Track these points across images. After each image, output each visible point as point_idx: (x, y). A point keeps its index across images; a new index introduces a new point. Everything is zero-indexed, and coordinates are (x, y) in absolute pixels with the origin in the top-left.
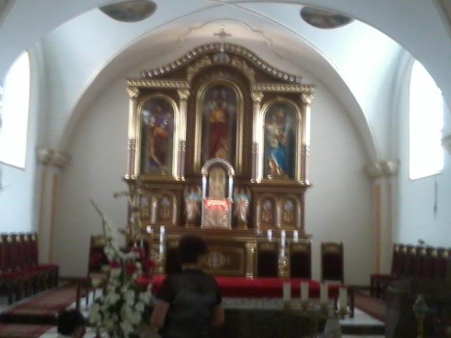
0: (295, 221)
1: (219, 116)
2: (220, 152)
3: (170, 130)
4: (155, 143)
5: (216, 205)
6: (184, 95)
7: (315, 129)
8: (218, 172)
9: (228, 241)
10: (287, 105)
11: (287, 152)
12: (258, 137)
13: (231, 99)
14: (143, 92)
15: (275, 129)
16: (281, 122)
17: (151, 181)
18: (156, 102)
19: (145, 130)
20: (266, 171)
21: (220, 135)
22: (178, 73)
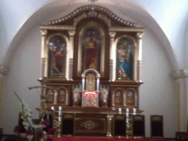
0: (133, 103)
1: (91, 45)
2: (92, 65)
3: (64, 53)
4: (56, 60)
5: (90, 94)
6: (72, 34)
7: (143, 52)
8: (91, 76)
9: (95, 114)
10: (128, 39)
11: (128, 64)
12: (113, 56)
13: (98, 35)
14: (50, 32)
15: (122, 52)
16: (125, 48)
17: (53, 81)
18: (56, 37)
19: (50, 53)
20: (118, 75)
21: (92, 56)
22: (69, 22)
